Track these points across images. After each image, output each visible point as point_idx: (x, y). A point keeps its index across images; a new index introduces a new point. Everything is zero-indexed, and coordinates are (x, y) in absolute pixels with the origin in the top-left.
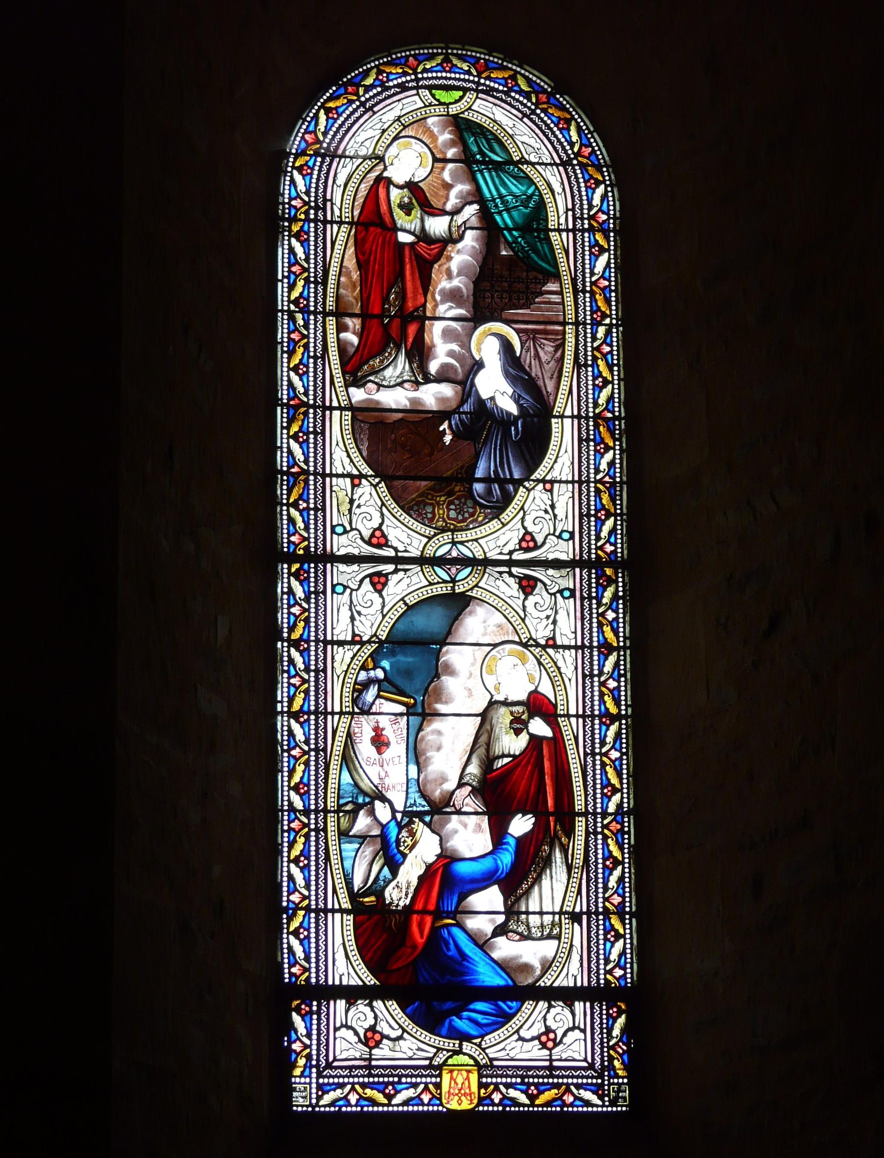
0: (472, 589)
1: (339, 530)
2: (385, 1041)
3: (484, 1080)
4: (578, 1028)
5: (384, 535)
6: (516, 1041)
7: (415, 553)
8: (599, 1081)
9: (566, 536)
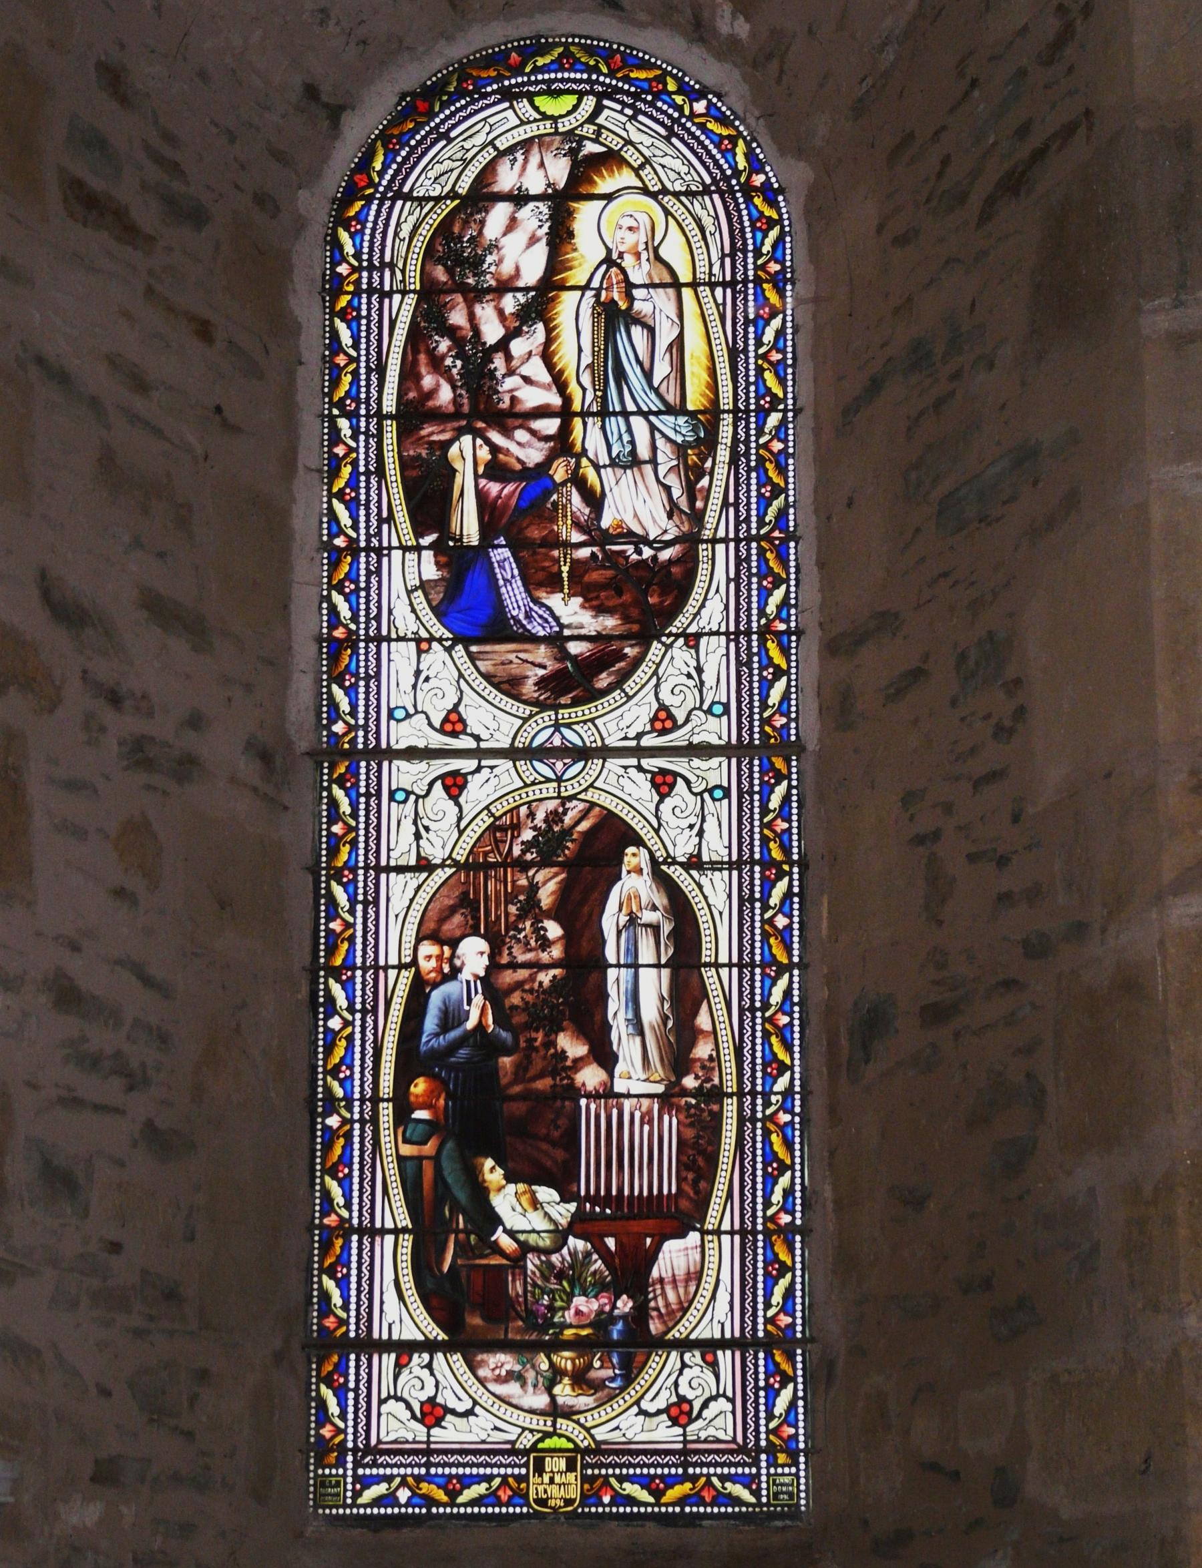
0: (586, 790)
1: (399, 714)
2: (449, 1417)
3: (589, 1472)
4: (724, 1395)
5: (461, 720)
6: (636, 1415)
7: (614, 764)
8: (754, 1470)
9: (718, 709)
